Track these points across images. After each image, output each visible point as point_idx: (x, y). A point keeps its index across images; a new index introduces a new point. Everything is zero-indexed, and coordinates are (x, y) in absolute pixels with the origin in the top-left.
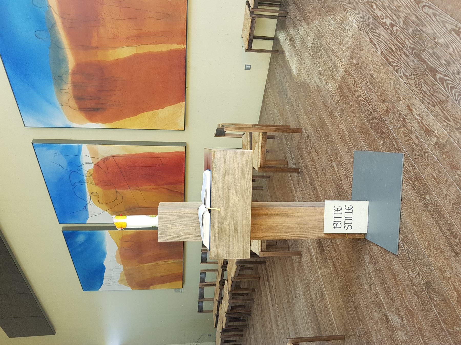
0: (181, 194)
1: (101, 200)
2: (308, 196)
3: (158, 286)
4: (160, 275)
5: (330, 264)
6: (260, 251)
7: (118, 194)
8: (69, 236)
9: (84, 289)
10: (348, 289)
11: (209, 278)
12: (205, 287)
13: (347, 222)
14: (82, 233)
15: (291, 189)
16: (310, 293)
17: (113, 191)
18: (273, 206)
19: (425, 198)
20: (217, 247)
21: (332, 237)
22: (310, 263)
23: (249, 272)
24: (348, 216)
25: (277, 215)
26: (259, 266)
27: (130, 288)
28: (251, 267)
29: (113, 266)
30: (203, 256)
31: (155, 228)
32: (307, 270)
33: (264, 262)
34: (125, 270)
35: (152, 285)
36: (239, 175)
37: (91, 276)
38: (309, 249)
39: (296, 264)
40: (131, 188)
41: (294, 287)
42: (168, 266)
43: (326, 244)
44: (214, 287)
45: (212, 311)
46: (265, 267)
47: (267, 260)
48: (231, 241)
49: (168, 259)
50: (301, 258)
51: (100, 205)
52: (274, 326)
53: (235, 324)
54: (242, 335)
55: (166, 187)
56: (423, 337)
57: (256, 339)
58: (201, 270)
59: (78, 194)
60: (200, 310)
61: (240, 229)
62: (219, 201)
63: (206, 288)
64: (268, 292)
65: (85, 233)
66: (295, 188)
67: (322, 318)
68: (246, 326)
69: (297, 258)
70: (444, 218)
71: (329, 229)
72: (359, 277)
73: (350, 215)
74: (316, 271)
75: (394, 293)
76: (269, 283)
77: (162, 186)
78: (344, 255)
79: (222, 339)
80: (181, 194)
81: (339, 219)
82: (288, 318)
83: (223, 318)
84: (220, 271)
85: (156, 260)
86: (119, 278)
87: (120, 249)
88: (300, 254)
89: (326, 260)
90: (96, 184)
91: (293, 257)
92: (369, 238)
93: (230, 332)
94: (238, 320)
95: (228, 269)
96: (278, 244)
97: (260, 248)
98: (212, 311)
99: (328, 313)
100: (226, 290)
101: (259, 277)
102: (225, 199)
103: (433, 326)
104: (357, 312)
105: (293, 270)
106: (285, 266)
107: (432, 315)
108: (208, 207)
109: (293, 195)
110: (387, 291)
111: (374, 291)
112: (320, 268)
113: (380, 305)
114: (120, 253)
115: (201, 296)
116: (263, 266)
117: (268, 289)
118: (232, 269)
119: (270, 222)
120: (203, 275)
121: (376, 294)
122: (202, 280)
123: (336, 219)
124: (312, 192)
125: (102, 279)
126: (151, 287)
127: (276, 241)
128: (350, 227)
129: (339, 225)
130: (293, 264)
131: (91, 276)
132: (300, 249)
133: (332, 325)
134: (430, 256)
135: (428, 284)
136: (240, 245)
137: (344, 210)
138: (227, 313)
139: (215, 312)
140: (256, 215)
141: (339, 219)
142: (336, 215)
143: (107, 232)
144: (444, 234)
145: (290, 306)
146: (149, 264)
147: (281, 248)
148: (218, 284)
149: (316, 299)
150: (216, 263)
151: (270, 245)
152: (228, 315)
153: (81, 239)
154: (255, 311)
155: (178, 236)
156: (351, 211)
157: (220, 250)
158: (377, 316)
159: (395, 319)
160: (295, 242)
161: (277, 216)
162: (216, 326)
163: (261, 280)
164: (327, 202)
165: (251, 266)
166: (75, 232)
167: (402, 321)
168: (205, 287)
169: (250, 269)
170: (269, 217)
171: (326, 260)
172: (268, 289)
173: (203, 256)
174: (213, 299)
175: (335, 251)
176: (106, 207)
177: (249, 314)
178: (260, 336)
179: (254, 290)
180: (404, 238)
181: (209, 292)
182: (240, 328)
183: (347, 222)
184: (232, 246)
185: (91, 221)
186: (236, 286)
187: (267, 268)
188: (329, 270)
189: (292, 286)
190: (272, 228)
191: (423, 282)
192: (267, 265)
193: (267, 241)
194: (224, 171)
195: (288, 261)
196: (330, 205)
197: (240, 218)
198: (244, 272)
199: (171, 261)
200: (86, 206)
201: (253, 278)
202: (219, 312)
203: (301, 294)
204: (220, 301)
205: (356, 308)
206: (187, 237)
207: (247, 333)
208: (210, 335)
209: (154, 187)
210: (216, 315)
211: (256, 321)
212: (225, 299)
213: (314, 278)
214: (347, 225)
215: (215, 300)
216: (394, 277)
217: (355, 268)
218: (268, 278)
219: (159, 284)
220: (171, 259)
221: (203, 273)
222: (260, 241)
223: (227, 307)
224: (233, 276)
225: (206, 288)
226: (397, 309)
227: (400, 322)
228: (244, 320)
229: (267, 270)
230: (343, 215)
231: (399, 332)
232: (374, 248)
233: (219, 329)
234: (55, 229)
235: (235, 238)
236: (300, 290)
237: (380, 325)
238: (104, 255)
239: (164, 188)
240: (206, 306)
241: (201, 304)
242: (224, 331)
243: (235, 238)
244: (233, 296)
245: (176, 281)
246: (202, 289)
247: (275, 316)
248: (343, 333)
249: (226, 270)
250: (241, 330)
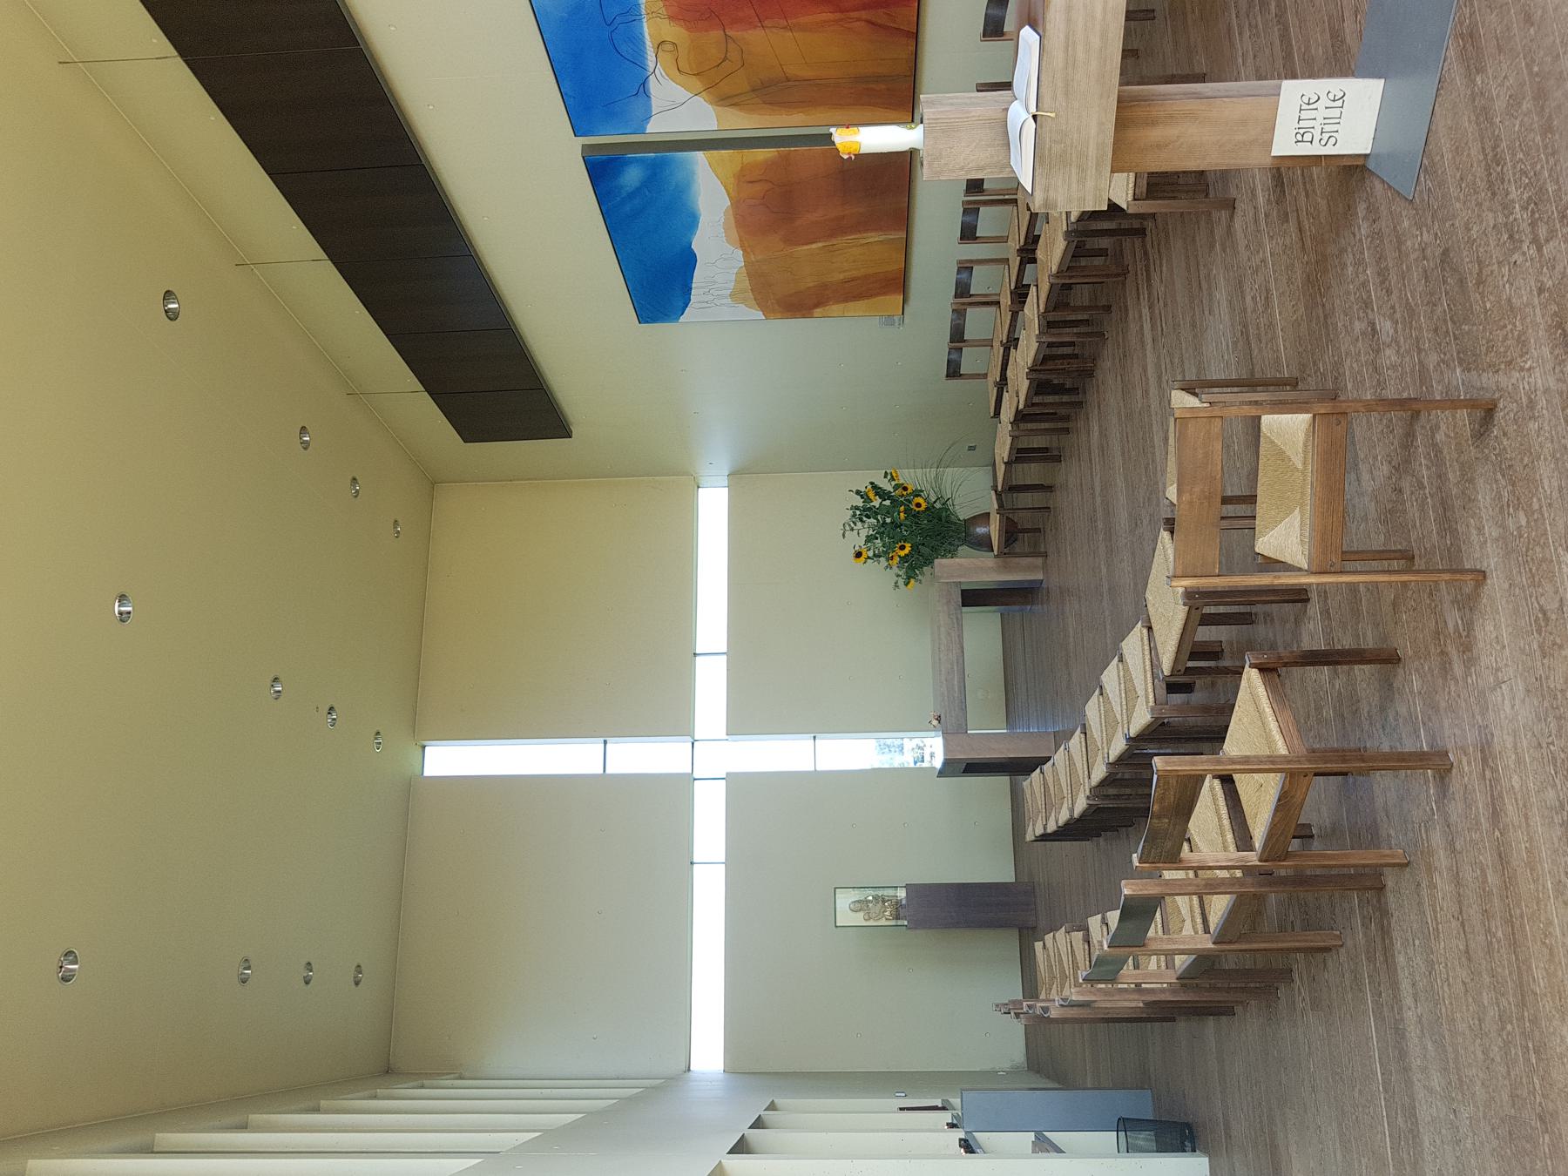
0: (908, 34)
1: (683, 65)
2: (1267, 51)
3: (835, 309)
4: (842, 276)
5: (1292, 226)
6: (1130, 198)
7: (731, 46)
8: (601, 169)
9: (642, 318)
10: (1317, 282)
11: (981, 282)
12: (969, 310)
13: (1327, 128)
14: (636, 160)
15: (1229, 29)
16: (1243, 298)
17: (716, 34)
18: (1166, 97)
19: (1473, 81)
20: (1047, 190)
21: (1289, 163)
22: (1251, 227)
23: (1098, 261)
24: (1330, 115)
25: (1171, 117)
26: (1127, 243)
27: (760, 315)
28: (1105, 240)
29: (717, 252)
30: (968, 219)
31: (911, 154)
32: (1242, 243)
33: (1141, 232)
34: (748, 264)
35: (817, 305)
36: (1096, 42)
37: (660, 284)
38: (1253, 191)
39: (1219, 232)
40: (766, 23)
41: (1210, 288)
42: (862, 251)
43: (1288, 175)
44: (993, 309)
45: (985, 376)
46: (1144, 246)
47: (1149, 225)
48: (1074, 178)
49: (866, 231)
50: (1232, 216)
51: (681, 78)
52: (1153, 390)
53: (1050, 399)
54: (1067, 431)
55: (864, 14)
56: (1420, 351)
57: (1103, 434)
58: (960, 262)
59: (623, 48)
60: (953, 371)
61: (1092, 151)
62: (1054, 98)
63: (971, 313)
64: (1146, 311)
65: (641, 161)
66: (1239, 26)
67: (1260, 350)
68: (1080, 404)
69: (1224, 214)
70: (1492, 124)
71: (1284, 145)
72: (1343, 251)
73: (1336, 113)
74: (1261, 245)
75: (1393, 278)
76: (1149, 286)
77: (855, 14)
78: (1323, 203)
79: (1014, 438)
80: (908, 34)
81: (1311, 124)
82: (1186, 366)
83: (1020, 383)
84: (1015, 262)
85: (832, 235)
86: (731, 285)
87: (736, 204)
88: (1231, 205)
89: (1285, 218)
90: (671, 18)
91: (1215, 215)
92: (1371, 165)
93: (1031, 421)
94: (1060, 389)
95: (1040, 254)
96: (1181, 181)
97: (1131, 192)
98: (985, 376)
99: (1274, 337)
100: (1032, 310)
101: (1125, 273)
102: (1067, 94)
103: (1436, 330)
104: (1326, 327)
105: (1212, 247)
106: (1194, 240)
107: (1440, 309)
108: (1033, 110)
109: (1232, 45)
110: (1383, 274)
111: (1362, 278)
112: (1271, 238)
113: (1367, 304)
114: (736, 215)
115: (957, 335)
116: (1138, 242)
117: (1144, 303)
118: (1053, 252)
119: (1156, 134)
120: (964, 276)
121: (1364, 284)
122: (962, 290)
123: (1302, 124)
124: (1277, 42)
125: (687, 290)
126: (818, 311)
127: (1177, 173)
128: (1332, 140)
129: (1308, 137)
130: (1212, 232)
131: (660, 284)
132: (1233, 193)
133: (1278, 360)
134: (1458, 199)
135: (1446, 252)
136: (1090, 184)
137: (1324, 102)
138: (1031, 370)
139: (995, 375)
140: (1127, 115)
141: (1311, 124)
142: (1304, 115)
143: (700, 156)
144: (1486, 155)
145: (1195, 336)
146: (814, 246)
147: (1183, 197)
148: (1006, 300)
149: (1254, 310)
150: (1003, 240)
151: (1158, 185)
152: (1034, 376)
153: (632, 177)
154: (1106, 364)
155: (962, 168)
156: (1339, 103)
157: (1052, 194)
158: (1358, 326)
159: (1386, 327)
160: (1224, 175)
161: (1171, 119)
162: (997, 413)
163: (1130, 277)
164: (1287, 85)
165: (1104, 243)
166: (611, 161)
167: (1396, 331)
168: (969, 310)
169: (1102, 253)
170: (1153, 123)
171: (1285, 218)
172: (1144, 303)
173: (968, 219)
174: (988, 343)
175: (1307, 196)
176: (697, 84)
177: (1090, 374)
178: (1115, 420)
179: (1108, 309)
180: (1427, 166)
181: (979, 322)
182: (1062, 411)
183: (1327, 128)
184: (1074, 186)
185: (660, 126)
186: (1060, 297)
187: (1149, 246)
188: (1288, 242)
189: (1204, 285)
190: (1159, 146)
191: (1439, 251)
192: (1148, 238)
193: (1151, 174)
194: (1067, 37)
195: (1203, 223)
196: (1293, 91)
197: (1093, 132)
198: (1083, 262)
199: (873, 237)
200: (644, 84)
201: (1108, 276)
202: (1009, 373)
203: (1224, 303)
204: (1012, 342)
205: (1326, 317)
206: (981, 169)
207: (1081, 424)
208: (972, 448)
209: (831, 16)
210: (996, 384)
211: (1108, 391)
212: (1029, 335)
213: (1256, 260)
214: (1326, 136)
215: (996, 344)
216: (1400, 243)
217: (1337, 235)
218: (1148, 271)
219: (838, 302)
220: (875, 230)
221: (966, 268)
222: (1132, 175)
223: (1032, 353)
224: (1054, 269)
225: (971, 313)
226: (1393, 307)
227: (1391, 332)
228: (1074, 390)
229: (1146, 253)
230: (1321, 114)
231: (1388, 352)
232: (1378, 186)
233: (1007, 414)
234: (563, 152)
235: (1082, 169)
236: (1221, 295)
237: (1360, 344)
238: (692, 222)
239: (858, 20)
240: (970, 360)
241: (954, 356)
242: (1020, 417)
243: (1082, 169)
244: (1048, 325)
245: (885, 294)
246: (959, 313)
247: (1158, 366)
248: (1296, 374)
249: (1034, 261)
250: (1067, 418)
